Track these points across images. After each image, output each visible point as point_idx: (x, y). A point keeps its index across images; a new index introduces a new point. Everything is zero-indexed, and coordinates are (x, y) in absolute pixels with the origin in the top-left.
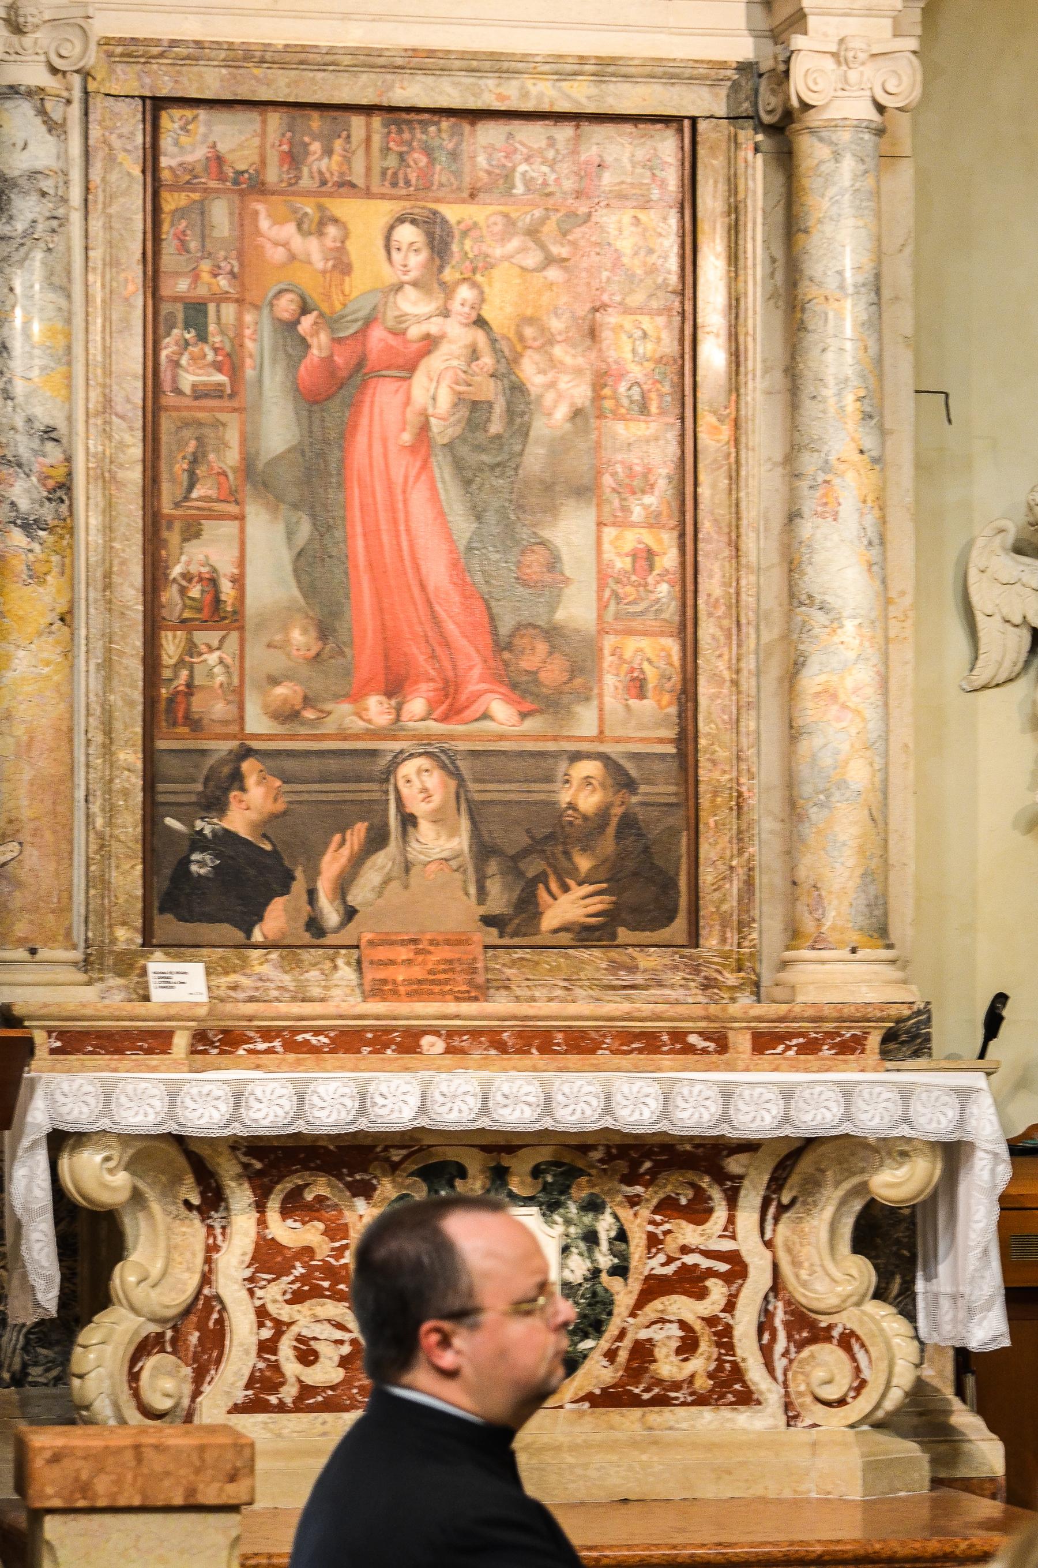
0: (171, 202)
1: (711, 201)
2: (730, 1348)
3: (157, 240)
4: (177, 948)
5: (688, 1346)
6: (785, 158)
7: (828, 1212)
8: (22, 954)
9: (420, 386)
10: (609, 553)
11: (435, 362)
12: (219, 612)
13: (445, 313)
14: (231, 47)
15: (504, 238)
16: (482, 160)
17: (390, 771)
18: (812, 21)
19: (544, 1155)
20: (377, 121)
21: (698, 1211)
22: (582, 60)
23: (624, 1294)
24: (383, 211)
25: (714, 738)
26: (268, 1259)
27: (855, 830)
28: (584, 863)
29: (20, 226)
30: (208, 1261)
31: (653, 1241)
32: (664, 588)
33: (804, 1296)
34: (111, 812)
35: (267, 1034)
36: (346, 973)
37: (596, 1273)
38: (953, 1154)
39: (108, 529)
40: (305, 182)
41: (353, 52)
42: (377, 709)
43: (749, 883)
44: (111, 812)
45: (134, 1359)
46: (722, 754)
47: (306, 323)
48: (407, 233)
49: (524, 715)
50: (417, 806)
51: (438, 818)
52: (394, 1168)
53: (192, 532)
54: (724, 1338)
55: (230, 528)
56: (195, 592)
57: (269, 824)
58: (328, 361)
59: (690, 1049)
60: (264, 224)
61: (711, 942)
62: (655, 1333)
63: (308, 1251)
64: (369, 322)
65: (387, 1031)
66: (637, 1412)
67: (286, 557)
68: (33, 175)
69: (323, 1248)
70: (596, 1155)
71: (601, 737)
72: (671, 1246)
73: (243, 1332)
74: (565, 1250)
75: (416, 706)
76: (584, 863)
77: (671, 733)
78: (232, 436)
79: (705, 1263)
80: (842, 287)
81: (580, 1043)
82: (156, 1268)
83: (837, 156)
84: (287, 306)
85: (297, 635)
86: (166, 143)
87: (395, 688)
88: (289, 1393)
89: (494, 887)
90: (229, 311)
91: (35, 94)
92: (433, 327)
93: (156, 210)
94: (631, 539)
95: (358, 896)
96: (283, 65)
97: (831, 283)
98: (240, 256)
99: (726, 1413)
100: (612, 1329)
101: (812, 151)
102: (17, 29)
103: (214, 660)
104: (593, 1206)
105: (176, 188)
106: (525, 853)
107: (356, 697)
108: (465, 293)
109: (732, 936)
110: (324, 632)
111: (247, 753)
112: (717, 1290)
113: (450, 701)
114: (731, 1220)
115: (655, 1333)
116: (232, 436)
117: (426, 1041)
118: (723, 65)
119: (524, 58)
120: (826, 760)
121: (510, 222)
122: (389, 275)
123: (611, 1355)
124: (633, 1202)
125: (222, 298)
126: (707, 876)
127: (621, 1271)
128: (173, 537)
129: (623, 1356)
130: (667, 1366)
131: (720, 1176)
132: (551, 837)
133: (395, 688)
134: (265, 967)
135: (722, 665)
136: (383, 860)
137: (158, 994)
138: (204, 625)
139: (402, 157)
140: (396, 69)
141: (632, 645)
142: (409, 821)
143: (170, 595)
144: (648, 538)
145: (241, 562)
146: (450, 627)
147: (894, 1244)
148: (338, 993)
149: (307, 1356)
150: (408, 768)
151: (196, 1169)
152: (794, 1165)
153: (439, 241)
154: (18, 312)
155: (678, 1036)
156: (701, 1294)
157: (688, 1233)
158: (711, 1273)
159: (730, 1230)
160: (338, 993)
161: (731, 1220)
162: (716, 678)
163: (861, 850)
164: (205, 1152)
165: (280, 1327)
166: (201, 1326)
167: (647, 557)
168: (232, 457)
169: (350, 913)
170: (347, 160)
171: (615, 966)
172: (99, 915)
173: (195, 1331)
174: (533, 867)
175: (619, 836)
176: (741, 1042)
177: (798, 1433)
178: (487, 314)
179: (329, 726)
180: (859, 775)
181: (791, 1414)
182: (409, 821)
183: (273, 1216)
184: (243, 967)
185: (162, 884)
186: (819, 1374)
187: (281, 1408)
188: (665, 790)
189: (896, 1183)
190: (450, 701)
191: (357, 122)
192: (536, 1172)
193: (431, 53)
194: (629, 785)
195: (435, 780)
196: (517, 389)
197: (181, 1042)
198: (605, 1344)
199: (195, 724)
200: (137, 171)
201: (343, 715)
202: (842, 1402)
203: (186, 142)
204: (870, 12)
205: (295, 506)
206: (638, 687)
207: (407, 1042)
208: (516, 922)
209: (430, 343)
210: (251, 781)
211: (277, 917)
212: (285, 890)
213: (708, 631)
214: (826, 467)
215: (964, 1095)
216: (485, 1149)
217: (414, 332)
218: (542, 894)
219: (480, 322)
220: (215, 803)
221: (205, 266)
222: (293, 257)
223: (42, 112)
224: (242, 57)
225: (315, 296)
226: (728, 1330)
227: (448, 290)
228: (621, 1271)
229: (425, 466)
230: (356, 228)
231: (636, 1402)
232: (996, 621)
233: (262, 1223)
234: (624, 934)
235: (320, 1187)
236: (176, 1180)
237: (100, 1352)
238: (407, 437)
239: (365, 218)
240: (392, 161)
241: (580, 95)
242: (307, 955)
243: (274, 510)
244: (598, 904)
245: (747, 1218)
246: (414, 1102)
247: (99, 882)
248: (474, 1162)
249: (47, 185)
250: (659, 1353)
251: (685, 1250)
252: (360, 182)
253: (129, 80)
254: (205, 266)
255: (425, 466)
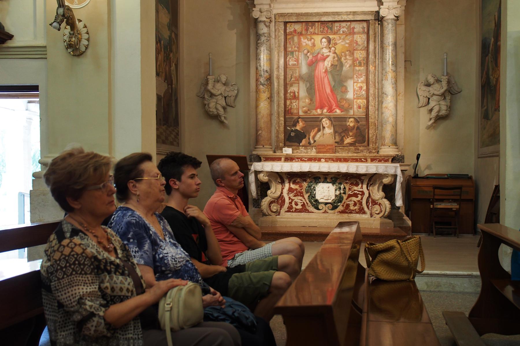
0: (288, 37)
1: (371, 32)
2: (362, 205)
3: (286, 43)
4: (289, 146)
5: (355, 205)
6: (382, 25)
7: (377, 185)
8: (262, 147)
9: (326, 63)
10: (355, 87)
11: (328, 59)
12: (295, 97)
13: (330, 52)
14: (296, 13)
15: (339, 40)
16: (336, 28)
17: (321, 121)
18: (384, 4)
19: (333, 176)
20: (319, 23)
21: (357, 185)
22: (351, 12)
23: (345, 197)
24: (320, 37)
25: (371, 115)
26: (290, 190)
27: (390, 128)
28: (351, 134)
29: (262, 41)
30: (282, 190)
31: (350, 189)
32: (364, 92)
33: (373, 198)
34: (279, 127)
35: (298, 158)
36: (314, 150)
37: (341, 193)
38: (395, 176)
39: (278, 85)
40: (309, 33)
41: (315, 13)
42: (319, 111)
43: (377, 137)
44: (279, 127)
45: (270, 204)
46: (373, 117)
47: (309, 54)
48: (324, 40)
49: (342, 112)
50: (325, 125)
51: (328, 127)
52: (310, 177)
53: (291, 85)
54: (361, 203)
55: (297, 85)
56: (292, 94)
57: (302, 128)
58: (312, 60)
59: (362, 161)
60: (302, 40)
61: (371, 146)
62: (350, 203)
63: (296, 189)
64: (318, 53)
65: (316, 158)
66: (347, 214)
67: (305, 89)
68: (264, 33)
69: (299, 189)
70: (341, 176)
71: (354, 115)
72: (352, 190)
73: (287, 201)
74: (336, 190)
75: (325, 111)
76: (351, 134)
77: (365, 114)
78: (297, 71)
79: (358, 192)
80: (389, 45)
81: (346, 160)
82: (274, 191)
83: (388, 24)
84: (306, 52)
85: (307, 100)
86: (288, 28)
87: (322, 108)
88: (294, 210)
89: (337, 137)
90: (297, 53)
91: (264, 22)
92: (328, 54)
93: (286, 38)
94: (359, 85)
95: (316, 139)
96: (305, 16)
97: (387, 44)
98: (299, 45)
99: (361, 215)
100: (343, 202)
101: (385, 24)
102: (261, 12)
103: (295, 104)
104: (340, 184)
105: (289, 35)
106: (342, 132)
107: (316, 109)
108: (333, 49)
109: (374, 145)
110: (311, 100)
111: (299, 118)
112: (360, 197)
113: (331, 110)
114: (362, 186)
115: (350, 203)
116: (297, 71)
117: (322, 160)
118: (373, 12)
119: (341, 12)
120: (386, 118)
121: (340, 38)
122: (321, 46)
123: (343, 206)
124: (347, 183)
125: (296, 51)
126: (370, 136)
127: (344, 193)
128: (288, 86)
129: (345, 206)
130: (352, 208)
131: (360, 179)
132: (346, 130)
133: (322, 108)
134: (302, 149)
135: (373, 104)
136: (320, 133)
137: (284, 153)
138: (293, 99)
139: (324, 28)
140: (322, 15)
141: (359, 101)
142: (324, 128)
143: (288, 95)
144: (361, 85)
145: (299, 90)
146: (330, 98)
147: (389, 191)
148: (313, 153)
149: (296, 204)
150: (324, 120)
151: (281, 177)
152: (372, 179)
153: (329, 41)
154: (262, 54)
155: (361, 159)
156: (357, 197)
157: (355, 188)
158: (359, 194)
159: (362, 188)
160: (313, 153)
161: (362, 186)
162: (372, 106)
163: (391, 131)
164: (281, 174)
165: (292, 200)
166: (281, 200)
167: (361, 88)
168: (297, 74)
169: (315, 141)
170: (315, 29)
171: (355, 149)
172: (278, 141)
173: (280, 200)
174: (343, 134)
175: (356, 130)
176: (369, 160)
177: (372, 218)
178: (336, 51)
179: (312, 114)
180: (391, 120)
181: (371, 216)
182: (324, 128)
183: (291, 184)
184: (299, 149)
185: (287, 137)
186: (375, 209)
187: (292, 212)
188: (364, 123)
189: (386, 181)
190: (331, 110)
191: (317, 24)
192: (331, 178)
193: (327, 13)
194: (358, 122)
195: (328, 122)
196: (341, 63)
197: (283, 159)
198: (342, 204)
199: (292, 114)
200: (283, 33)
201: (314, 112)
202: (379, 214)
203: (290, 28)
204: (393, 1)
205: (307, 81)
206: (359, 107)
207: (319, 160)
208: (340, 143)
209: (328, 56)
210: (300, 122)
211: (304, 142)
212: (305, 138)
213: (371, 98)
214: (386, 72)
215: (396, 167)
216: (324, 175)
217: (325, 55)
218: (344, 139)
219: (335, 53)
220: (295, 125)
221: (293, 46)
222: (306, 44)
223: (265, 24)
224: (298, 15)
225: (310, 50)
226: (362, 202)
227: (330, 48)
228: (344, 193)
229: (327, 75)
230: (316, 40)
231: (347, 213)
232: (422, 97)
233: (290, 185)
234: (357, 144)
235: (298, 180)
236: (277, 179)
237: (265, 202)
238: (324, 71)
239: (317, 38)
240: (322, 29)
241: (351, 18)
242: (308, 147)
243: (304, 82)
244: (353, 140)
245: (365, 186)
246: (309, 167)
247: (277, 137)
248: (322, 177)
249: (266, 35)
250: (351, 206)
251: (355, 190)
252: (317, 33)
253: (282, 19)
254: (293, 46)
255: (327, 75)
